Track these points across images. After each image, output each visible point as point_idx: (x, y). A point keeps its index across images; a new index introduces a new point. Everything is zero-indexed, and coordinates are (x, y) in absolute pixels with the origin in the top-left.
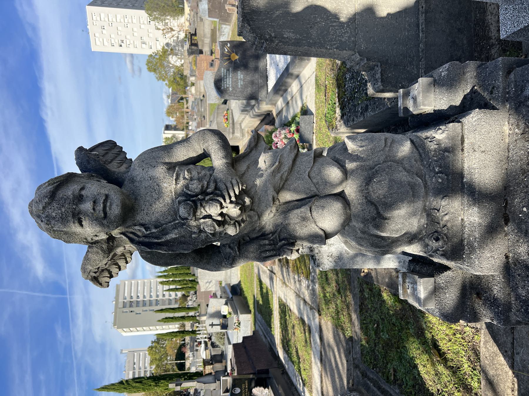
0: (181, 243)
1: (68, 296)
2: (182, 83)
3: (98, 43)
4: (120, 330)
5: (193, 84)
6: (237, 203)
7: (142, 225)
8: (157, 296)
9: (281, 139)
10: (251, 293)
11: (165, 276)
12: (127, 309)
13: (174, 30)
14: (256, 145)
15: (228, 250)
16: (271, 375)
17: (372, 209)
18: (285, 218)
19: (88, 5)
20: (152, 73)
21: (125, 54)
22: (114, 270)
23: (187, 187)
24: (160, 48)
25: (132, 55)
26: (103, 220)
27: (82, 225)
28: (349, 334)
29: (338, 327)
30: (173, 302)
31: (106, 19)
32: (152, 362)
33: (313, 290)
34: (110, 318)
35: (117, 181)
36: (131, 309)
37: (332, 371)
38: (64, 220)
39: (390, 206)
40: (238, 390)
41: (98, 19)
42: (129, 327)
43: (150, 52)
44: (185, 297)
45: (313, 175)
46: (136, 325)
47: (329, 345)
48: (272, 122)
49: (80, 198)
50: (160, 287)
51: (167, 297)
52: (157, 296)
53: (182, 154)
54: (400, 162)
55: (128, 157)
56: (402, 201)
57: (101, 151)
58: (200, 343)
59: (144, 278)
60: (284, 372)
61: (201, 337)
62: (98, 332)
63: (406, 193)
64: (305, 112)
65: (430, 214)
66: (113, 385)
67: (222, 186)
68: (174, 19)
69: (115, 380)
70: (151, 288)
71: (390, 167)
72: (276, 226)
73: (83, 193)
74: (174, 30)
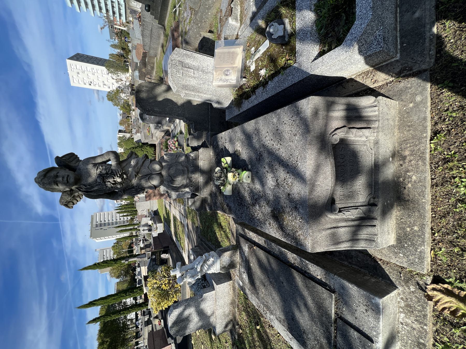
0: (100, 191)
1: (60, 223)
2: (128, 108)
3: (75, 81)
4: (94, 239)
5: (134, 110)
6: (120, 177)
7: (84, 185)
8: (116, 220)
9: (141, 154)
10: (162, 214)
11: (120, 209)
12: (99, 228)
13: (123, 81)
14: (131, 156)
15: (120, 193)
16: (170, 248)
17: (170, 178)
18: (140, 181)
19: (68, 59)
20: (111, 102)
21: (94, 90)
22: (75, 202)
23: (101, 172)
24: (115, 88)
25: (98, 91)
26: (67, 183)
27: (58, 186)
28: (196, 225)
29: (193, 223)
30: (126, 222)
31: (80, 69)
32: (114, 254)
33: (185, 209)
34: (88, 233)
35: (73, 169)
36: (101, 228)
37: (192, 241)
38: (50, 184)
39: (175, 177)
40: (154, 257)
41: (75, 68)
42: (100, 237)
43: (109, 90)
44: (132, 219)
45: (149, 167)
46: (104, 235)
47: (191, 231)
48: (169, 135)
49: (57, 176)
50: (118, 215)
51: (122, 220)
52: (116, 220)
53: (99, 160)
54: (180, 163)
55: (80, 159)
56: (179, 175)
57: (67, 157)
58: (140, 241)
59: (108, 211)
60: (176, 246)
61: (141, 238)
62: (81, 241)
63: (182, 173)
64: (181, 133)
65: (190, 179)
66: (90, 266)
67: (114, 171)
68: (123, 74)
69: (91, 264)
70: (112, 216)
71: (176, 165)
72: (137, 184)
73: (58, 174)
74: (123, 81)
